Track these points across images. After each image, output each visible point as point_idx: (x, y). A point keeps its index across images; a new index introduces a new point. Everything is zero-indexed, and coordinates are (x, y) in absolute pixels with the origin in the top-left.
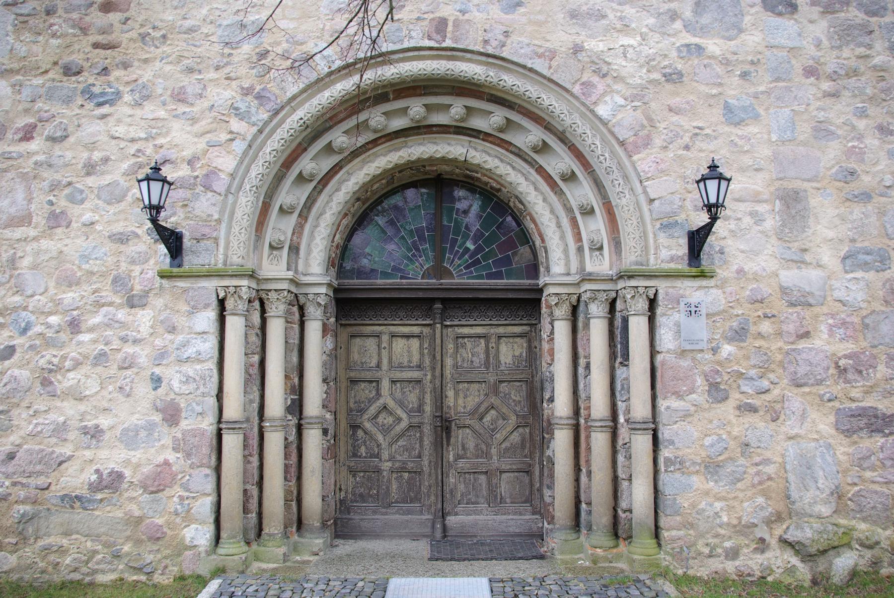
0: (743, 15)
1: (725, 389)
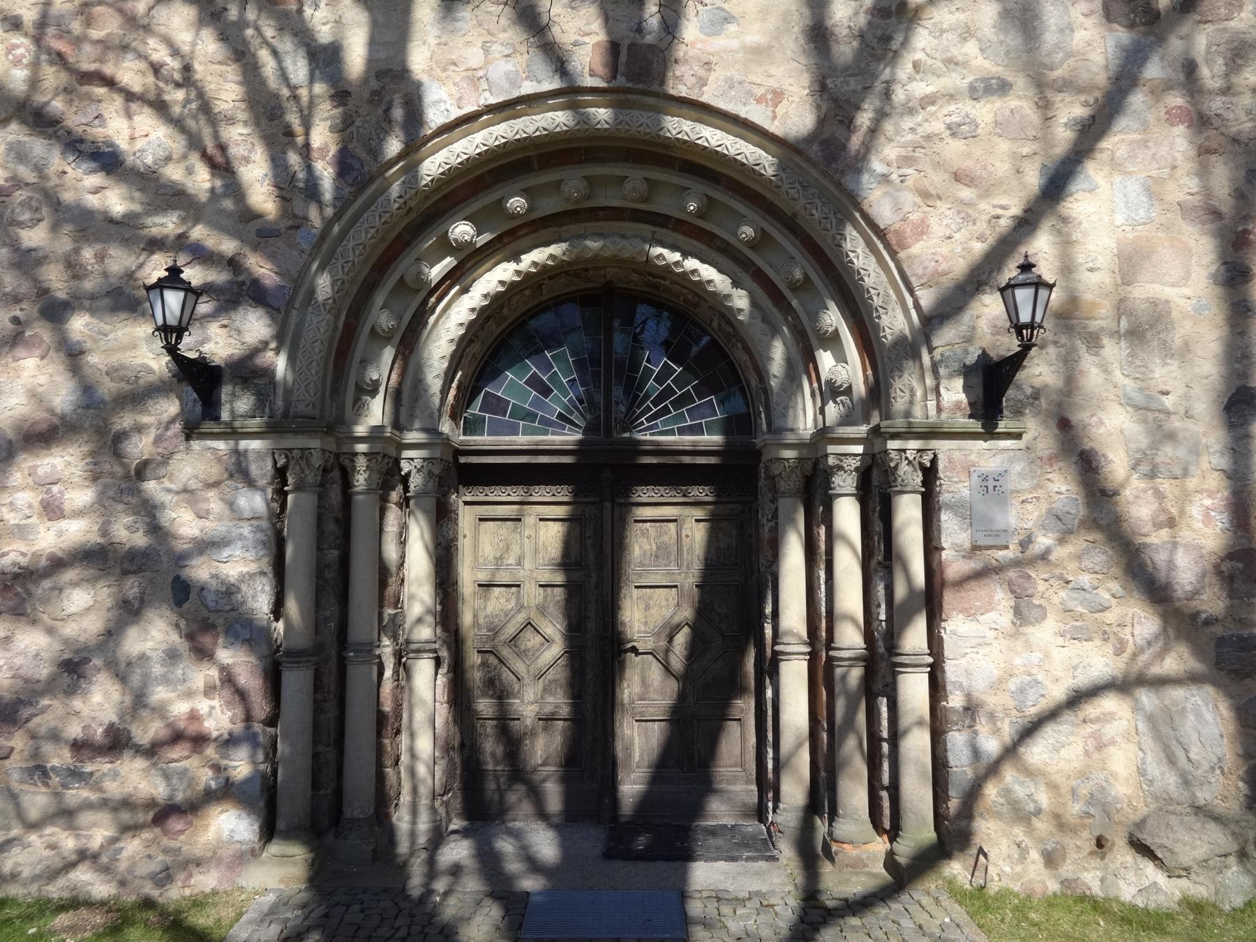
0: (1073, 31)
1: (1040, 606)
